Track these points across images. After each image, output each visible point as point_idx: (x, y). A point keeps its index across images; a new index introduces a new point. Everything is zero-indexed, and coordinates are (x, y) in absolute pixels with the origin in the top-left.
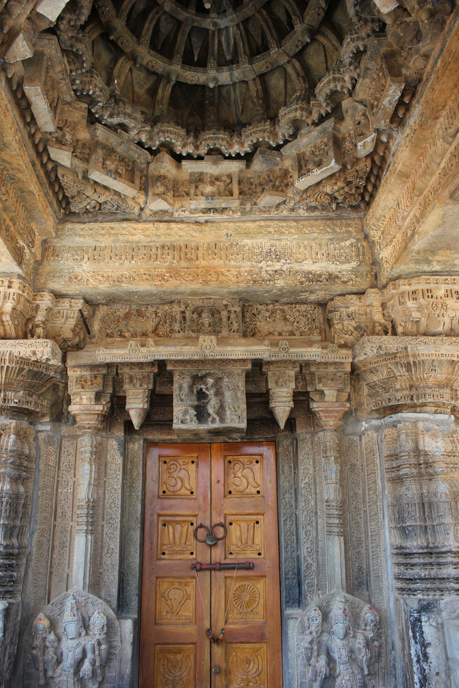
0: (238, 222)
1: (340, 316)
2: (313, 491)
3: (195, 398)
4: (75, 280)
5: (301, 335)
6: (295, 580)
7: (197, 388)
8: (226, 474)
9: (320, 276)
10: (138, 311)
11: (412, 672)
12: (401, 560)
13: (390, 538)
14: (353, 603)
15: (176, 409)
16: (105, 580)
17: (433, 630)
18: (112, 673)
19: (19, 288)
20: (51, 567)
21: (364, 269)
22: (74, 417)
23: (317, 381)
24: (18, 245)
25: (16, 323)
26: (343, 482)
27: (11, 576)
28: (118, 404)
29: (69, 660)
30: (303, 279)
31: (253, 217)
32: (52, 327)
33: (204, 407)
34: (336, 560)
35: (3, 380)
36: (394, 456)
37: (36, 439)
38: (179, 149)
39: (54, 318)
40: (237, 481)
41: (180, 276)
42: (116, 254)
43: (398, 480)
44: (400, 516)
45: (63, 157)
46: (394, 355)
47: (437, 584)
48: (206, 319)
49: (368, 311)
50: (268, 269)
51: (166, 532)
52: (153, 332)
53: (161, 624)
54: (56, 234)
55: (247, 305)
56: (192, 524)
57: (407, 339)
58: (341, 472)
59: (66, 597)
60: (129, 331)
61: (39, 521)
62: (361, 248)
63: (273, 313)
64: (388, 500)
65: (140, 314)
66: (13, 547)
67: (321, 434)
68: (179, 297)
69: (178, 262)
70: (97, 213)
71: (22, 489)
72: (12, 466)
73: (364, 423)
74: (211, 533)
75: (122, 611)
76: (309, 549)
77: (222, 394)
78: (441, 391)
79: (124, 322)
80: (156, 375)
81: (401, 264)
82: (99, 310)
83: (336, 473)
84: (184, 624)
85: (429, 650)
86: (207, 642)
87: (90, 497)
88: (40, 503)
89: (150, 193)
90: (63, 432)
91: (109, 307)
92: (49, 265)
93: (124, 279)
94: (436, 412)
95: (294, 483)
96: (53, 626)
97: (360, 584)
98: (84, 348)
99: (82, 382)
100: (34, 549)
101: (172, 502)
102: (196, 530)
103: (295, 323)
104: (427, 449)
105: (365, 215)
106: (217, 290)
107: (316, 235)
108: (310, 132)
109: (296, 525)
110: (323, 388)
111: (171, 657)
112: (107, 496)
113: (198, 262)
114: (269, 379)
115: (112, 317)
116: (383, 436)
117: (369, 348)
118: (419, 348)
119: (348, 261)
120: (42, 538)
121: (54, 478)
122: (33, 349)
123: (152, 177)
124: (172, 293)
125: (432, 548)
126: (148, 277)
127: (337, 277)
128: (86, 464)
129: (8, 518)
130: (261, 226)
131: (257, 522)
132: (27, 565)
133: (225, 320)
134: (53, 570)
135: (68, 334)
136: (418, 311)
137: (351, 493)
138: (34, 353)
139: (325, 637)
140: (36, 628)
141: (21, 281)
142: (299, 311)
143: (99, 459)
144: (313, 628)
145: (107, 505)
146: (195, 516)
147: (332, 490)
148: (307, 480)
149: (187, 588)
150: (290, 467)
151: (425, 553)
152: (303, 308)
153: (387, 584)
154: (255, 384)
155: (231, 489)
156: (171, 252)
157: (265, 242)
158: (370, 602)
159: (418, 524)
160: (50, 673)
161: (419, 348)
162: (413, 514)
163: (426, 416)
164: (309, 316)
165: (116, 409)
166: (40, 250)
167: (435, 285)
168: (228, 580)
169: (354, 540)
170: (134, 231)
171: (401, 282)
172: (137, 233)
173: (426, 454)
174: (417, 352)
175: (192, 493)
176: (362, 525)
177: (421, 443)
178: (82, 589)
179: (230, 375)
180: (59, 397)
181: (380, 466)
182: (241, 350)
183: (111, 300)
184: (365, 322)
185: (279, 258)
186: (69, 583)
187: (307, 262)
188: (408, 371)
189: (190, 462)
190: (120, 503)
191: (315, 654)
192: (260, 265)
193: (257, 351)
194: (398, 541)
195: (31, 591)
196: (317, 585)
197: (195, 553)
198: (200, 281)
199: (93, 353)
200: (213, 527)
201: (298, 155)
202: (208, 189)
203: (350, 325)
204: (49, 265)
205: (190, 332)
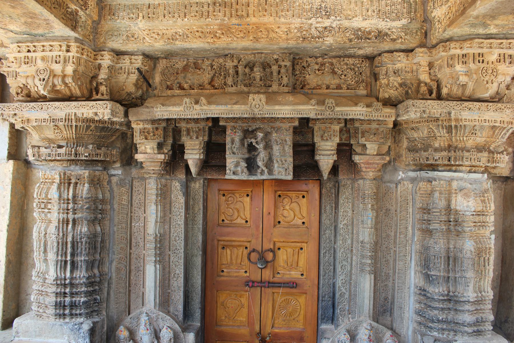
1: (387, 72)
2: (350, 231)
3: (245, 150)
4: (132, 39)
5: (348, 89)
6: (330, 303)
7: (248, 141)
8: (276, 207)
9: (369, 33)
10: (194, 63)
13: (415, 279)
14: (377, 329)
16: (173, 298)
19: (77, 52)
20: (129, 286)
21: (415, 26)
23: (360, 136)
24: (69, 10)
25: (79, 83)
27: (95, 299)
30: (353, 36)
32: (116, 82)
33: (254, 159)
34: (366, 294)
35: (74, 136)
37: (109, 182)
39: (117, 74)
40: (285, 213)
41: (232, 33)
43: (428, 232)
44: (426, 263)
48: (258, 73)
49: (415, 68)
50: (318, 25)
51: (225, 254)
52: (210, 84)
53: (220, 326)
55: (297, 57)
56: (246, 248)
57: (451, 105)
58: (377, 217)
59: (141, 313)
60: (187, 83)
61: (116, 252)
63: (322, 65)
64: (416, 247)
65: (197, 66)
67: (361, 182)
68: (232, 52)
69: (229, 19)
72: (88, 211)
73: (401, 173)
75: (188, 320)
76: (344, 281)
78: (479, 155)
79: (182, 75)
80: (210, 128)
81: (455, 28)
82: (159, 63)
83: (372, 218)
87: (157, 233)
88: (116, 237)
90: (133, 174)
91: (168, 61)
92: (107, 24)
93: (178, 37)
94: (470, 172)
95: (335, 221)
97: (385, 311)
98: (147, 99)
100: (114, 275)
101: (230, 230)
102: (249, 254)
103: (343, 76)
104: (458, 208)
106: (267, 46)
109: (334, 257)
110: (366, 143)
112: (172, 230)
113: (248, 19)
114: (315, 134)
115: (171, 70)
116: (418, 189)
117: (413, 113)
118: (462, 113)
119: (398, 18)
120: (120, 265)
121: (127, 215)
122: (95, 110)
124: (224, 49)
125: (451, 296)
126: (201, 34)
127: (386, 34)
128: (153, 204)
129: (88, 254)
131: (302, 249)
132: (109, 287)
133: (275, 74)
134: (131, 288)
135: (131, 88)
136: (465, 75)
137: (384, 235)
138: (96, 114)
141: (78, 44)
142: (347, 64)
143: (165, 199)
145: (173, 238)
146: (249, 242)
147: (367, 234)
148: (345, 222)
149: (242, 299)
150: (332, 207)
151: (445, 300)
152: (351, 61)
153: (408, 316)
154: (303, 135)
155: (280, 220)
156: (222, 9)
158: (392, 329)
159: (442, 274)
161: (462, 113)
162: (438, 265)
164: (357, 69)
165: (176, 158)
166: (96, 10)
167: (488, 50)
169: (383, 274)
171: (453, 45)
174: (460, 117)
175: (247, 221)
176: (391, 263)
177: (453, 202)
178: (153, 307)
179: (278, 130)
180: (127, 144)
182: (290, 109)
183: (169, 55)
184: (410, 79)
185: (329, 15)
187: (357, 19)
188: (448, 133)
189: (245, 195)
190: (183, 236)
192: (310, 22)
195: (114, 308)
196: (348, 310)
197: (248, 272)
198: (251, 38)
199: (152, 109)
203: (395, 81)
204: (107, 24)
205: (243, 87)
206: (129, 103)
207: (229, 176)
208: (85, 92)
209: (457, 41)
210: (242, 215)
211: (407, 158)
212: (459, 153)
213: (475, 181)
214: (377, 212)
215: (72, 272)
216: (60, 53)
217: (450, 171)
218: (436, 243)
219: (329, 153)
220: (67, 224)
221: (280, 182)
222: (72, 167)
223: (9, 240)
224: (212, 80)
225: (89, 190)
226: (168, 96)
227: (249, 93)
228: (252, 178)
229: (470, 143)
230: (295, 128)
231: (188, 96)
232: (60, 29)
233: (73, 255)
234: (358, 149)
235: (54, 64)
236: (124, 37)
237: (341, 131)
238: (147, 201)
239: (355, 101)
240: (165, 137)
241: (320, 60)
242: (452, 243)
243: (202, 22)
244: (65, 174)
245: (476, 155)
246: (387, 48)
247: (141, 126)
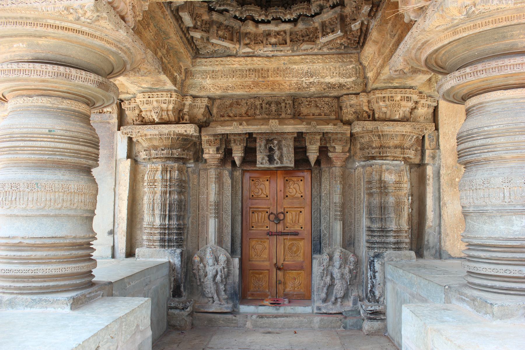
0: (290, 56)
3: (268, 151)
8: (285, 187)
9: (335, 85)
11: (368, 283)
12: (370, 233)
15: (258, 157)
17: (379, 266)
18: (230, 281)
21: (360, 80)
22: (206, 160)
26: (344, 194)
27: (181, 238)
28: (228, 153)
29: (210, 275)
31: (298, 53)
36: (370, 182)
37: (187, 171)
38: (257, 18)
40: (291, 190)
41: (259, 86)
42: (224, 75)
43: (371, 195)
45: (197, 35)
46: (372, 131)
47: (385, 245)
48: (273, 108)
49: (361, 103)
50: (306, 81)
54: (192, 65)
56: (267, 212)
62: (358, 69)
64: (365, 204)
65: (238, 104)
66: (181, 225)
67: (334, 168)
68: (259, 96)
70: (213, 55)
71: (183, 197)
74: (277, 217)
77: (282, 149)
84: (263, 261)
85: (376, 274)
86: (275, 270)
89: (242, 44)
94: (393, 160)
96: (202, 260)
97: (350, 244)
99: (209, 142)
101: (257, 201)
102: (269, 215)
104: (385, 180)
105: (361, 51)
107: (332, 63)
108: (328, 12)
109: (320, 214)
111: (257, 276)
113: (268, 79)
114: (306, 141)
123: (243, 33)
127: (344, 85)
130: (302, 59)
131: (301, 212)
132: (188, 233)
133: (283, 108)
135: (200, 117)
137: (348, 199)
138: (186, 131)
139: (330, 268)
140: (194, 261)
142: (324, 101)
143: (220, 181)
144: (325, 264)
146: (269, 208)
147: (338, 198)
152: (327, 99)
157: (305, 67)
160: (202, 280)
163: (388, 162)
165: (227, 156)
168: (286, 240)
170: (234, 63)
171: (377, 92)
172: (236, 63)
173: (385, 182)
176: (353, 216)
177: (383, 176)
179: (286, 139)
181: (363, 186)
182: (292, 128)
183: (221, 98)
186: (117, 170)
191: (325, 275)
193: (299, 128)
194: (369, 224)
199: (215, 128)
200: (277, 214)
201: (322, 22)
202: (273, 40)
203: (351, 110)
206: (202, 126)
207: (259, 165)
208: (177, 119)
209: (379, 90)
210: (264, 192)
212: (385, 149)
213: (396, 165)
214: (343, 186)
215: (169, 221)
216: (167, 98)
217: (382, 160)
218: (374, 199)
219: (314, 151)
220: (166, 194)
221: (287, 172)
222: (168, 162)
223: (128, 205)
224: (247, 111)
225: (178, 174)
226: (221, 121)
227: (269, 119)
228: (272, 166)
229: (391, 143)
230: (295, 138)
231: (235, 120)
232: (170, 85)
233: (169, 211)
234: (331, 150)
235: (163, 104)
236: (199, 88)
237: (321, 139)
238: (208, 183)
240: (221, 144)
241: (309, 99)
242: (383, 199)
243: (243, 80)
244: (164, 165)
245: (393, 150)
246: (345, 93)
247: (207, 138)
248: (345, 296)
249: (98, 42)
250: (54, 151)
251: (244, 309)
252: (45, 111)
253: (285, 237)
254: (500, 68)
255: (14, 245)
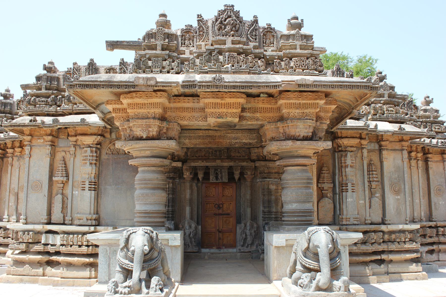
8: (223, 191)
26: (251, 195)
28: (196, 175)
36: (263, 189)
43: (264, 195)
44: (264, 203)
48: (218, 153)
99: (187, 170)
119: (254, 140)
152: (243, 149)
165: (195, 177)
194: (263, 209)
207: (211, 181)
211: (259, 175)
221: (224, 183)
228: (217, 182)
229: (273, 171)
234: (246, 173)
237: (241, 168)
239: (243, 160)
245: (274, 174)
248: (252, 244)
249: (171, 150)
250: (158, 184)
251: (204, 250)
252: (153, 172)
253: (223, 216)
254: (289, 162)
255: (140, 212)
